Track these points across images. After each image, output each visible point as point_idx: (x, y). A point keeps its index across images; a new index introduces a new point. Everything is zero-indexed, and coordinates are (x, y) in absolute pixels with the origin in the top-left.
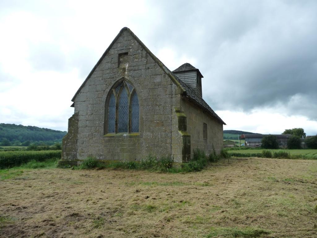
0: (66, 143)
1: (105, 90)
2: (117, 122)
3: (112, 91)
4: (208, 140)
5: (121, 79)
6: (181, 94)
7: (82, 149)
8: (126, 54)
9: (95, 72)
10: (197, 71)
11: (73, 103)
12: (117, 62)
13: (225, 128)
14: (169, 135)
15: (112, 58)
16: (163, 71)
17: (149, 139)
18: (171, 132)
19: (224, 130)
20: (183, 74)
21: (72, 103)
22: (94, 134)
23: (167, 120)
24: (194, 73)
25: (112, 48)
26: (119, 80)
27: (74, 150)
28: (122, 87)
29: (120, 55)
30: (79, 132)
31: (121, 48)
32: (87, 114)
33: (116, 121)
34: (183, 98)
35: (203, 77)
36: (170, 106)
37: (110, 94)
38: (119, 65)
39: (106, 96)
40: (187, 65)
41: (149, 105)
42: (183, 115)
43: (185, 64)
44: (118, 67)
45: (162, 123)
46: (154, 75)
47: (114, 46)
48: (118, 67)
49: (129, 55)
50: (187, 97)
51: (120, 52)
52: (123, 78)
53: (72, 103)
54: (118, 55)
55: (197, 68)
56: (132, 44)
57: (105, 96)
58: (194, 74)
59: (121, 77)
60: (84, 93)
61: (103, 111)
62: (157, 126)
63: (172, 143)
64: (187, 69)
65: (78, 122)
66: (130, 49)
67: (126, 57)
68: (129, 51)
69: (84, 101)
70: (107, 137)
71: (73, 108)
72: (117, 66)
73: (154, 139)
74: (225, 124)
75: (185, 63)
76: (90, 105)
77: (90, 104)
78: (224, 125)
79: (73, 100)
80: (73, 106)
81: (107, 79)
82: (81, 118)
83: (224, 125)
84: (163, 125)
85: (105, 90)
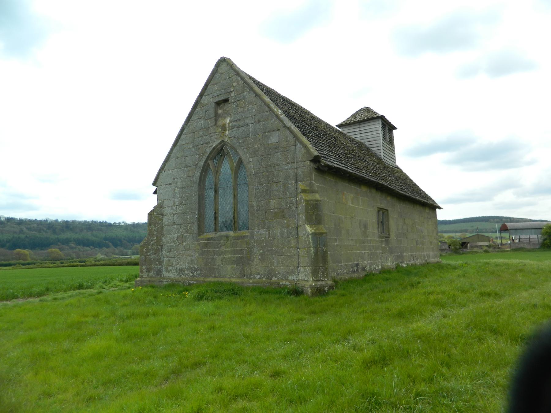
0: (146, 252)
1: (198, 164)
2: (217, 215)
3: (208, 164)
4: (393, 236)
5: (220, 143)
6: (311, 161)
7: (169, 260)
8: (226, 101)
9: (183, 137)
10: (382, 118)
11: (156, 187)
12: (214, 116)
13: (441, 215)
14: (294, 232)
15: (206, 111)
16: (281, 124)
17: (263, 240)
18: (297, 228)
19: (437, 219)
20: (358, 126)
21: (154, 188)
22: (184, 235)
23: (290, 207)
24: (377, 122)
25: (206, 94)
26: (217, 146)
27: (157, 263)
28: (222, 158)
29: (218, 104)
30: (165, 233)
31: (219, 93)
32: (174, 205)
33: (215, 213)
34: (316, 167)
35: (395, 128)
36: (293, 182)
37: (205, 170)
38: (216, 121)
39: (199, 174)
40: (367, 110)
41: (262, 184)
42: (317, 197)
43: (359, 111)
44: (216, 124)
45: (283, 212)
46: (269, 132)
47: (208, 91)
48: (216, 124)
49: (229, 102)
50: (323, 164)
51: (218, 99)
52: (223, 141)
53: (154, 188)
54: (214, 104)
55: (381, 113)
56: (234, 84)
57: (198, 174)
58: (378, 125)
59: (220, 141)
60: (169, 170)
61: (195, 199)
62: (275, 219)
63: (299, 247)
64: (366, 116)
65: (163, 218)
66: (231, 92)
67: (226, 106)
68: (229, 96)
69: (170, 184)
70: (202, 239)
71: (156, 195)
72: (214, 123)
73: (271, 240)
74: (440, 208)
75: (362, 107)
76: (179, 189)
77: (178, 188)
78: (437, 210)
79: (154, 184)
80: (155, 193)
81: (199, 146)
82: (167, 211)
83: (437, 210)
84: (283, 217)
85: (198, 164)
